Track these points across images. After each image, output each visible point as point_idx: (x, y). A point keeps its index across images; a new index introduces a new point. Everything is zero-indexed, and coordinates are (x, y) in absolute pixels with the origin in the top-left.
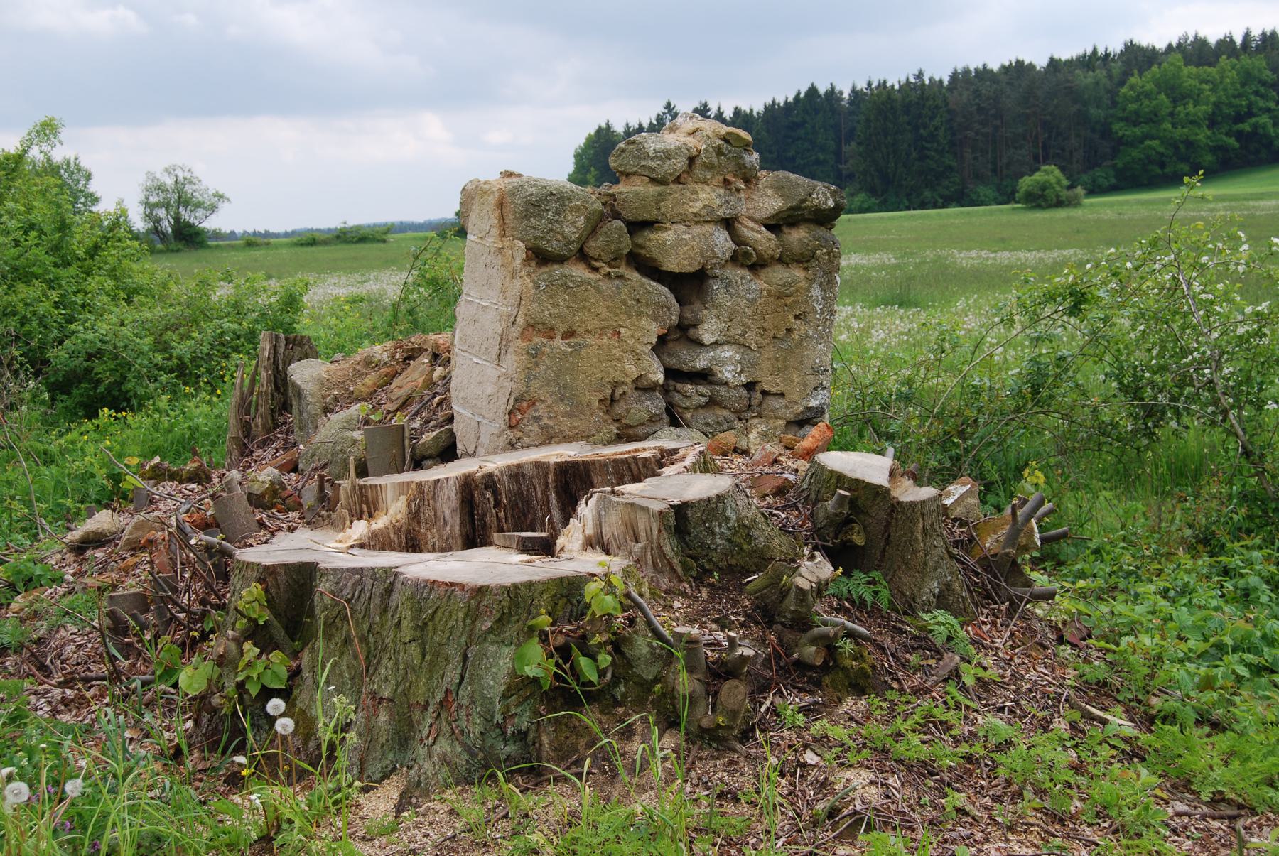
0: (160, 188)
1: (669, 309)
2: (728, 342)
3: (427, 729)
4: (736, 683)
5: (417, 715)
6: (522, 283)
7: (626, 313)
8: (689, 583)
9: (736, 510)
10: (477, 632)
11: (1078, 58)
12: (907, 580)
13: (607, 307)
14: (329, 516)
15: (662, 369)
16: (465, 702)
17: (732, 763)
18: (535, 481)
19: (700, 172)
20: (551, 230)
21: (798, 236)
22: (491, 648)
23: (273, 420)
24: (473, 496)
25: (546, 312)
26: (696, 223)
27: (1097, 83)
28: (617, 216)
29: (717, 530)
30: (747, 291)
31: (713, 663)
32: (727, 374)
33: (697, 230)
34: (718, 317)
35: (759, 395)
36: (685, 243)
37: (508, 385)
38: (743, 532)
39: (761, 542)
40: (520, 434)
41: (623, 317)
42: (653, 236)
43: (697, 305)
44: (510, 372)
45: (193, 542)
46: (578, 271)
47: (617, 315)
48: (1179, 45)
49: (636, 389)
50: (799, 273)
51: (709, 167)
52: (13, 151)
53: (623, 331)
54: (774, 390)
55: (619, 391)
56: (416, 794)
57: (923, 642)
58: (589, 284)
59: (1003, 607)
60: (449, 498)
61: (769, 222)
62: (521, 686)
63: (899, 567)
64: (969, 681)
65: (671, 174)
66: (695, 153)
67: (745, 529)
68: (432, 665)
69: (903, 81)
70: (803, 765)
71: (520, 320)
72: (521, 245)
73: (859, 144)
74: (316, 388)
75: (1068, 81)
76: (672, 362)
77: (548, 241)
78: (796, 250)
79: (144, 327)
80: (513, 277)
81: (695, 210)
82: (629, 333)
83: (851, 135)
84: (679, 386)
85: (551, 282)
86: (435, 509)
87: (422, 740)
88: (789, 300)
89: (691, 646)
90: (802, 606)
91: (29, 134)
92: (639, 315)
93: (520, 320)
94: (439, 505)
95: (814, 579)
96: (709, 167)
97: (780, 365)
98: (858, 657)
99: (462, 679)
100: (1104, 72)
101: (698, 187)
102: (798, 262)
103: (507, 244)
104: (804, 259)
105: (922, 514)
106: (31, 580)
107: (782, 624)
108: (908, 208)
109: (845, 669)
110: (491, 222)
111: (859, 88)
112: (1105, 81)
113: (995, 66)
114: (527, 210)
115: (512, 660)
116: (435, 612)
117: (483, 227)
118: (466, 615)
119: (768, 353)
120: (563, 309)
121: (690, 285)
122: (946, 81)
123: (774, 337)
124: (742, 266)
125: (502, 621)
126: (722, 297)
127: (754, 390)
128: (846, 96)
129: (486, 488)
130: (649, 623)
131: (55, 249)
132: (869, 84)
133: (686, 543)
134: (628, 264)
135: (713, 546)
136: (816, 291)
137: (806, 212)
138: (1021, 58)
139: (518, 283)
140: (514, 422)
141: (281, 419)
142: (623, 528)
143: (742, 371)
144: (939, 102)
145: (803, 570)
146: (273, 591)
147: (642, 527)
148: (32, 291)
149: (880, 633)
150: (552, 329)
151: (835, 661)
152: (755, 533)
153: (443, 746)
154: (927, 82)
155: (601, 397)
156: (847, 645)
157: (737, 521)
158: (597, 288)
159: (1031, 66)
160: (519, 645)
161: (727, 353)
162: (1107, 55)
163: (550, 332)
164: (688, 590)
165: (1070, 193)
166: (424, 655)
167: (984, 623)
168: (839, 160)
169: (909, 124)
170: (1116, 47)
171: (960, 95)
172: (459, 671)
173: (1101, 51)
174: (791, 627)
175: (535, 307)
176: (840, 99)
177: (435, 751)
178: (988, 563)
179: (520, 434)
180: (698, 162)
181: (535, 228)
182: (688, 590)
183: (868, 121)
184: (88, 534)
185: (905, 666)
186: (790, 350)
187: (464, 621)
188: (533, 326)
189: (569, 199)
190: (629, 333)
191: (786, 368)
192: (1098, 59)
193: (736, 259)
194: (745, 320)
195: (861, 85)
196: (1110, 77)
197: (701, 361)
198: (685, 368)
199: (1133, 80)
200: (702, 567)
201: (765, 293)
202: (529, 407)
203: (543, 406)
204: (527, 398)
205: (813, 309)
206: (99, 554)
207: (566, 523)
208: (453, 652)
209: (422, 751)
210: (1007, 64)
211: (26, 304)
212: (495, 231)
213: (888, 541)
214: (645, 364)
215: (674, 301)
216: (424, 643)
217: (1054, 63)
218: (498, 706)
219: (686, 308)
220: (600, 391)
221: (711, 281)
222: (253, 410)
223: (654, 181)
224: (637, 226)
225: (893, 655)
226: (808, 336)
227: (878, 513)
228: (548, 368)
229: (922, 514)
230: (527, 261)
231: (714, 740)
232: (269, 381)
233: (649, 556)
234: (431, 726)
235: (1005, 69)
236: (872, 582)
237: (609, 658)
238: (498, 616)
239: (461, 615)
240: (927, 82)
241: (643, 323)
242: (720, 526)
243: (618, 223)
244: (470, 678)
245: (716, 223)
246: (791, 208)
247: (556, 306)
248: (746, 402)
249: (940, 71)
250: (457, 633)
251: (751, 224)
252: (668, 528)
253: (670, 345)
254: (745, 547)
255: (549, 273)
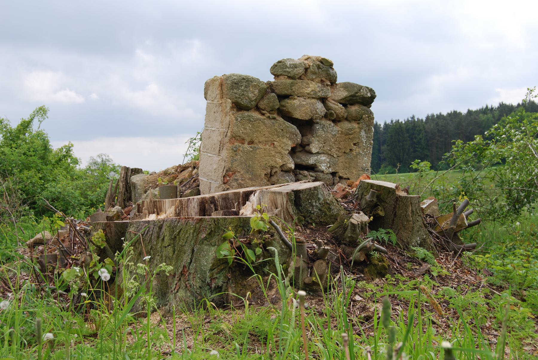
0: (95, 163)
1: (296, 136)
2: (324, 153)
3: (175, 286)
4: (321, 261)
5: (170, 280)
6: (231, 117)
7: (277, 135)
8: (301, 226)
9: (323, 195)
10: (199, 239)
11: (480, 110)
12: (404, 234)
13: (268, 131)
14: (139, 215)
15: (293, 162)
16: (192, 271)
17: (320, 301)
18: (234, 201)
19: (310, 75)
20: (243, 94)
21: (354, 109)
22: (206, 247)
23: (124, 204)
24: (205, 207)
25: (241, 131)
26: (309, 98)
27: (488, 120)
28: (273, 91)
29: (314, 204)
30: (332, 131)
31: (311, 255)
32: (323, 167)
33: (309, 101)
34: (319, 141)
35: (338, 178)
36: (304, 106)
37: (223, 164)
38: (327, 206)
39: (335, 212)
40: (228, 187)
41: (276, 137)
42: (289, 101)
43: (309, 136)
44: (224, 158)
45: (78, 228)
46: (256, 115)
47: (273, 135)
48: (523, 104)
49: (282, 171)
50: (355, 125)
51: (314, 73)
52: (27, 120)
53: (275, 143)
54: (345, 176)
55: (274, 171)
56: (168, 315)
57: (413, 260)
58: (260, 120)
59: (451, 253)
60: (194, 207)
61: (341, 102)
62: (221, 263)
63: (401, 228)
64: (435, 274)
65: (297, 75)
66: (308, 66)
67: (327, 205)
68: (178, 256)
69: (406, 120)
70: (355, 301)
71: (229, 134)
72: (229, 100)
73: (388, 146)
74: (142, 183)
75: (475, 119)
76: (298, 161)
77: (242, 100)
78: (354, 115)
79: (77, 188)
80: (226, 115)
81: (308, 92)
82: (278, 144)
83: (384, 142)
84: (301, 172)
85: (243, 118)
86: (187, 212)
87: (172, 291)
88: (351, 137)
89: (300, 244)
90: (354, 234)
91: (34, 112)
92: (283, 136)
93: (229, 134)
94: (189, 210)
95: (360, 221)
96: (314, 73)
97: (347, 165)
98: (381, 260)
99: (191, 261)
100: (492, 115)
101: (309, 82)
102: (355, 120)
103: (223, 101)
104: (357, 119)
105: (411, 203)
106: (9, 259)
107: (345, 244)
108: (409, 172)
109: (375, 265)
110: (217, 93)
111: (387, 123)
112: (491, 119)
113: (445, 113)
114: (232, 86)
115: (215, 252)
116: (180, 231)
117: (214, 95)
118: (194, 231)
119: (342, 159)
120: (248, 131)
121: (306, 126)
122: (424, 119)
123: (345, 153)
124: (330, 120)
125: (211, 234)
126: (320, 132)
127: (336, 176)
128: (382, 126)
129: (211, 203)
130: (281, 237)
131: (43, 158)
132: (392, 121)
133: (300, 211)
134: (278, 114)
135: (312, 212)
136: (363, 133)
137: (358, 98)
138: (455, 110)
139: (228, 118)
140: (226, 181)
141: (128, 204)
142: (270, 204)
143: (330, 167)
144: (421, 128)
145: (354, 217)
146: (109, 235)
147: (279, 202)
148: (32, 173)
149: (392, 255)
150: (243, 139)
151: (370, 262)
152: (332, 207)
153: (181, 293)
154: (416, 120)
155: (265, 172)
156: (377, 255)
157: (324, 200)
158: (265, 124)
159: (460, 113)
160: (218, 246)
161: (323, 158)
162: (492, 108)
163: (242, 141)
164: (300, 230)
165: (478, 165)
166: (174, 252)
167: (442, 259)
168: (380, 153)
169: (409, 137)
170: (496, 105)
171: (430, 125)
172: (190, 257)
173: (489, 107)
174: (349, 246)
175: (235, 129)
176: (380, 128)
177: (179, 296)
178: (442, 233)
179: (228, 187)
180: (309, 70)
181: (236, 93)
182: (300, 230)
183: (391, 136)
184: (36, 239)
185: (404, 268)
186: (352, 159)
187: (193, 234)
188: (235, 137)
189: (252, 82)
190: (278, 144)
191: (350, 167)
192: (489, 110)
193: (326, 116)
194: (331, 144)
195: (388, 122)
196: (494, 117)
197: (311, 161)
198: (304, 163)
199: (503, 118)
200: (308, 222)
201: (340, 132)
202: (232, 174)
203: (239, 174)
204: (232, 170)
205: (362, 141)
206: (41, 248)
207: (244, 204)
208: (188, 249)
209: (172, 297)
210: (450, 112)
211: (27, 178)
212: (219, 96)
213: (395, 215)
214: (286, 159)
215: (299, 132)
216: (174, 246)
217: (470, 112)
218: (208, 274)
219: (304, 138)
220: (265, 170)
221: (316, 125)
222: (116, 200)
223: (289, 77)
224: (282, 97)
225: (398, 263)
226: (360, 153)
227: (391, 201)
228: (241, 157)
229: (411, 203)
230: (232, 108)
231: (311, 291)
232: (123, 187)
233: (282, 215)
234: (176, 284)
235: (449, 115)
236: (388, 233)
237: (261, 250)
238: (209, 231)
239: (192, 231)
240: (416, 120)
241: (285, 140)
242: (316, 202)
243: (274, 94)
244: (195, 260)
245: (318, 99)
246: (351, 96)
247: (245, 129)
248: (332, 181)
249: (422, 116)
250: (190, 239)
251: (333, 102)
252: (291, 201)
253: (298, 154)
254: (328, 213)
255: (242, 114)
